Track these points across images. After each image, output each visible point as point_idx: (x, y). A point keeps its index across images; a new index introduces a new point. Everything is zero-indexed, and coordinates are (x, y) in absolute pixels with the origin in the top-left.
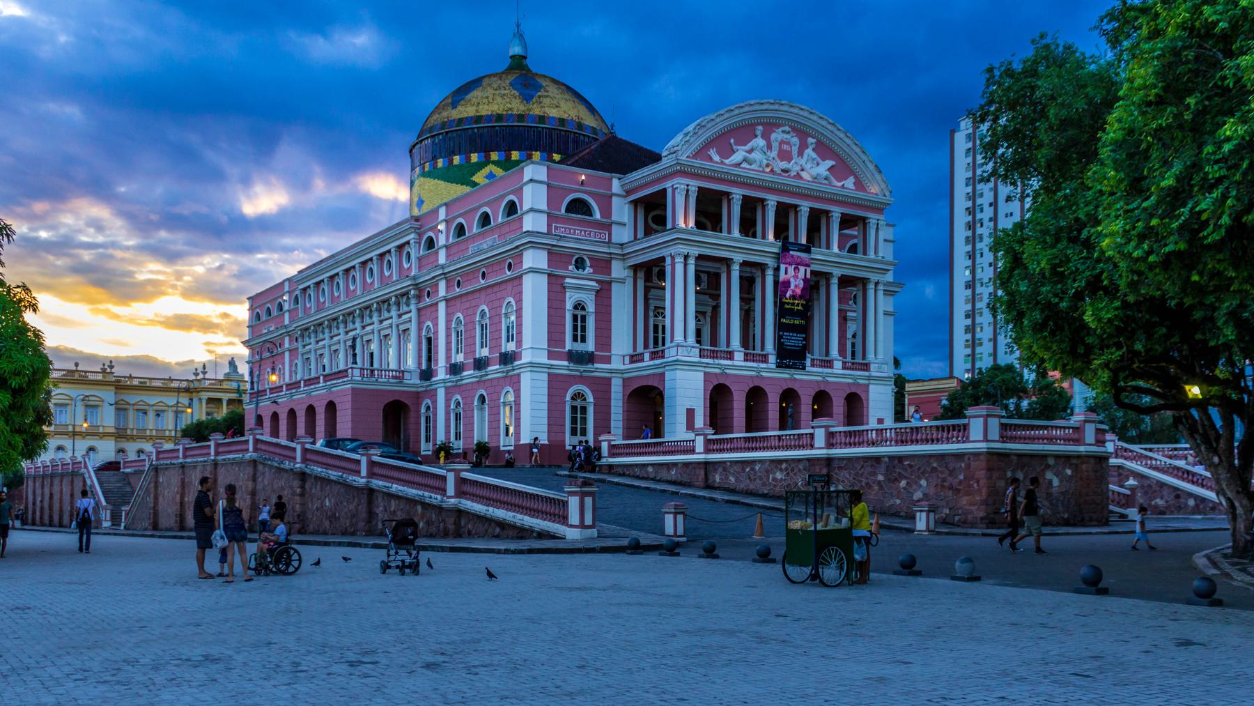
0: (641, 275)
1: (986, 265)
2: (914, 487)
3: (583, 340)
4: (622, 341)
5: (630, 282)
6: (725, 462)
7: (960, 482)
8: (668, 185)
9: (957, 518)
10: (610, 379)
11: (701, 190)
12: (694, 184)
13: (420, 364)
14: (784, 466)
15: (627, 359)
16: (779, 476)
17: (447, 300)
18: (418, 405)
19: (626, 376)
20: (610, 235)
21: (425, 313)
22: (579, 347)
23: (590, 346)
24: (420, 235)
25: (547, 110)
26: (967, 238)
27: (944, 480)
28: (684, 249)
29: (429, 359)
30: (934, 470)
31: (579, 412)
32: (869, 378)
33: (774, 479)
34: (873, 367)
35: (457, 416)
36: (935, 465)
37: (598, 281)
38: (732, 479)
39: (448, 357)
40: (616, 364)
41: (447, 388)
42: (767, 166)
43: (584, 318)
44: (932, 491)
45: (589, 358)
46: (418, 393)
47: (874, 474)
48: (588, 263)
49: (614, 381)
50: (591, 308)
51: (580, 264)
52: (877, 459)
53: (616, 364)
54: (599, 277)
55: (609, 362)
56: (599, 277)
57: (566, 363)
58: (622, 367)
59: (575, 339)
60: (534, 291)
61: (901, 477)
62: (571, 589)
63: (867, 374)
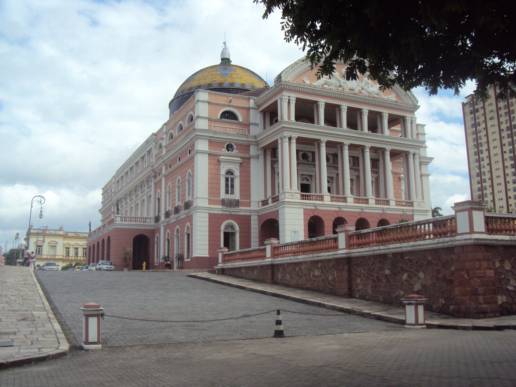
0: (269, 153)
1: (486, 165)
2: (414, 279)
3: (232, 193)
4: (257, 193)
5: (261, 158)
6: (283, 264)
7: (453, 273)
8: (277, 98)
9: (452, 307)
10: (250, 216)
11: (298, 100)
12: (294, 96)
13: (155, 214)
14: (319, 265)
15: (260, 204)
16: (317, 273)
17: (165, 176)
18: (154, 237)
19: (260, 214)
20: (249, 131)
21: (158, 185)
22: (229, 197)
23: (237, 196)
24: (157, 143)
25: (234, 80)
26: (475, 152)
27: (438, 272)
28: (287, 134)
29: (159, 211)
30: (429, 263)
31: (228, 237)
32: (413, 211)
33: (314, 276)
34: (415, 204)
35: (169, 240)
36: (430, 258)
37: (241, 158)
38: (288, 276)
39: (166, 208)
40: (254, 207)
41: (164, 226)
42: (340, 86)
43: (232, 180)
44: (429, 283)
45: (237, 203)
46: (154, 230)
47: (382, 269)
48: (235, 147)
49: (252, 218)
50: (237, 173)
51: (229, 147)
52: (384, 256)
53: (254, 207)
54: (242, 155)
55: (250, 206)
56: (242, 155)
57: (221, 207)
58: (258, 209)
59: (227, 192)
60: (202, 165)
61: (403, 270)
62: (257, 338)
63: (411, 208)
